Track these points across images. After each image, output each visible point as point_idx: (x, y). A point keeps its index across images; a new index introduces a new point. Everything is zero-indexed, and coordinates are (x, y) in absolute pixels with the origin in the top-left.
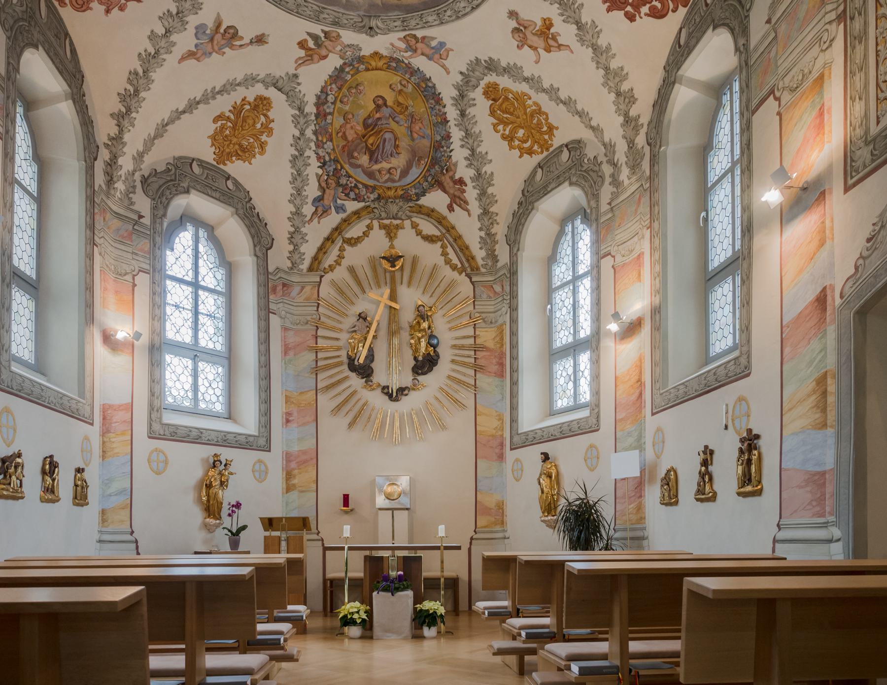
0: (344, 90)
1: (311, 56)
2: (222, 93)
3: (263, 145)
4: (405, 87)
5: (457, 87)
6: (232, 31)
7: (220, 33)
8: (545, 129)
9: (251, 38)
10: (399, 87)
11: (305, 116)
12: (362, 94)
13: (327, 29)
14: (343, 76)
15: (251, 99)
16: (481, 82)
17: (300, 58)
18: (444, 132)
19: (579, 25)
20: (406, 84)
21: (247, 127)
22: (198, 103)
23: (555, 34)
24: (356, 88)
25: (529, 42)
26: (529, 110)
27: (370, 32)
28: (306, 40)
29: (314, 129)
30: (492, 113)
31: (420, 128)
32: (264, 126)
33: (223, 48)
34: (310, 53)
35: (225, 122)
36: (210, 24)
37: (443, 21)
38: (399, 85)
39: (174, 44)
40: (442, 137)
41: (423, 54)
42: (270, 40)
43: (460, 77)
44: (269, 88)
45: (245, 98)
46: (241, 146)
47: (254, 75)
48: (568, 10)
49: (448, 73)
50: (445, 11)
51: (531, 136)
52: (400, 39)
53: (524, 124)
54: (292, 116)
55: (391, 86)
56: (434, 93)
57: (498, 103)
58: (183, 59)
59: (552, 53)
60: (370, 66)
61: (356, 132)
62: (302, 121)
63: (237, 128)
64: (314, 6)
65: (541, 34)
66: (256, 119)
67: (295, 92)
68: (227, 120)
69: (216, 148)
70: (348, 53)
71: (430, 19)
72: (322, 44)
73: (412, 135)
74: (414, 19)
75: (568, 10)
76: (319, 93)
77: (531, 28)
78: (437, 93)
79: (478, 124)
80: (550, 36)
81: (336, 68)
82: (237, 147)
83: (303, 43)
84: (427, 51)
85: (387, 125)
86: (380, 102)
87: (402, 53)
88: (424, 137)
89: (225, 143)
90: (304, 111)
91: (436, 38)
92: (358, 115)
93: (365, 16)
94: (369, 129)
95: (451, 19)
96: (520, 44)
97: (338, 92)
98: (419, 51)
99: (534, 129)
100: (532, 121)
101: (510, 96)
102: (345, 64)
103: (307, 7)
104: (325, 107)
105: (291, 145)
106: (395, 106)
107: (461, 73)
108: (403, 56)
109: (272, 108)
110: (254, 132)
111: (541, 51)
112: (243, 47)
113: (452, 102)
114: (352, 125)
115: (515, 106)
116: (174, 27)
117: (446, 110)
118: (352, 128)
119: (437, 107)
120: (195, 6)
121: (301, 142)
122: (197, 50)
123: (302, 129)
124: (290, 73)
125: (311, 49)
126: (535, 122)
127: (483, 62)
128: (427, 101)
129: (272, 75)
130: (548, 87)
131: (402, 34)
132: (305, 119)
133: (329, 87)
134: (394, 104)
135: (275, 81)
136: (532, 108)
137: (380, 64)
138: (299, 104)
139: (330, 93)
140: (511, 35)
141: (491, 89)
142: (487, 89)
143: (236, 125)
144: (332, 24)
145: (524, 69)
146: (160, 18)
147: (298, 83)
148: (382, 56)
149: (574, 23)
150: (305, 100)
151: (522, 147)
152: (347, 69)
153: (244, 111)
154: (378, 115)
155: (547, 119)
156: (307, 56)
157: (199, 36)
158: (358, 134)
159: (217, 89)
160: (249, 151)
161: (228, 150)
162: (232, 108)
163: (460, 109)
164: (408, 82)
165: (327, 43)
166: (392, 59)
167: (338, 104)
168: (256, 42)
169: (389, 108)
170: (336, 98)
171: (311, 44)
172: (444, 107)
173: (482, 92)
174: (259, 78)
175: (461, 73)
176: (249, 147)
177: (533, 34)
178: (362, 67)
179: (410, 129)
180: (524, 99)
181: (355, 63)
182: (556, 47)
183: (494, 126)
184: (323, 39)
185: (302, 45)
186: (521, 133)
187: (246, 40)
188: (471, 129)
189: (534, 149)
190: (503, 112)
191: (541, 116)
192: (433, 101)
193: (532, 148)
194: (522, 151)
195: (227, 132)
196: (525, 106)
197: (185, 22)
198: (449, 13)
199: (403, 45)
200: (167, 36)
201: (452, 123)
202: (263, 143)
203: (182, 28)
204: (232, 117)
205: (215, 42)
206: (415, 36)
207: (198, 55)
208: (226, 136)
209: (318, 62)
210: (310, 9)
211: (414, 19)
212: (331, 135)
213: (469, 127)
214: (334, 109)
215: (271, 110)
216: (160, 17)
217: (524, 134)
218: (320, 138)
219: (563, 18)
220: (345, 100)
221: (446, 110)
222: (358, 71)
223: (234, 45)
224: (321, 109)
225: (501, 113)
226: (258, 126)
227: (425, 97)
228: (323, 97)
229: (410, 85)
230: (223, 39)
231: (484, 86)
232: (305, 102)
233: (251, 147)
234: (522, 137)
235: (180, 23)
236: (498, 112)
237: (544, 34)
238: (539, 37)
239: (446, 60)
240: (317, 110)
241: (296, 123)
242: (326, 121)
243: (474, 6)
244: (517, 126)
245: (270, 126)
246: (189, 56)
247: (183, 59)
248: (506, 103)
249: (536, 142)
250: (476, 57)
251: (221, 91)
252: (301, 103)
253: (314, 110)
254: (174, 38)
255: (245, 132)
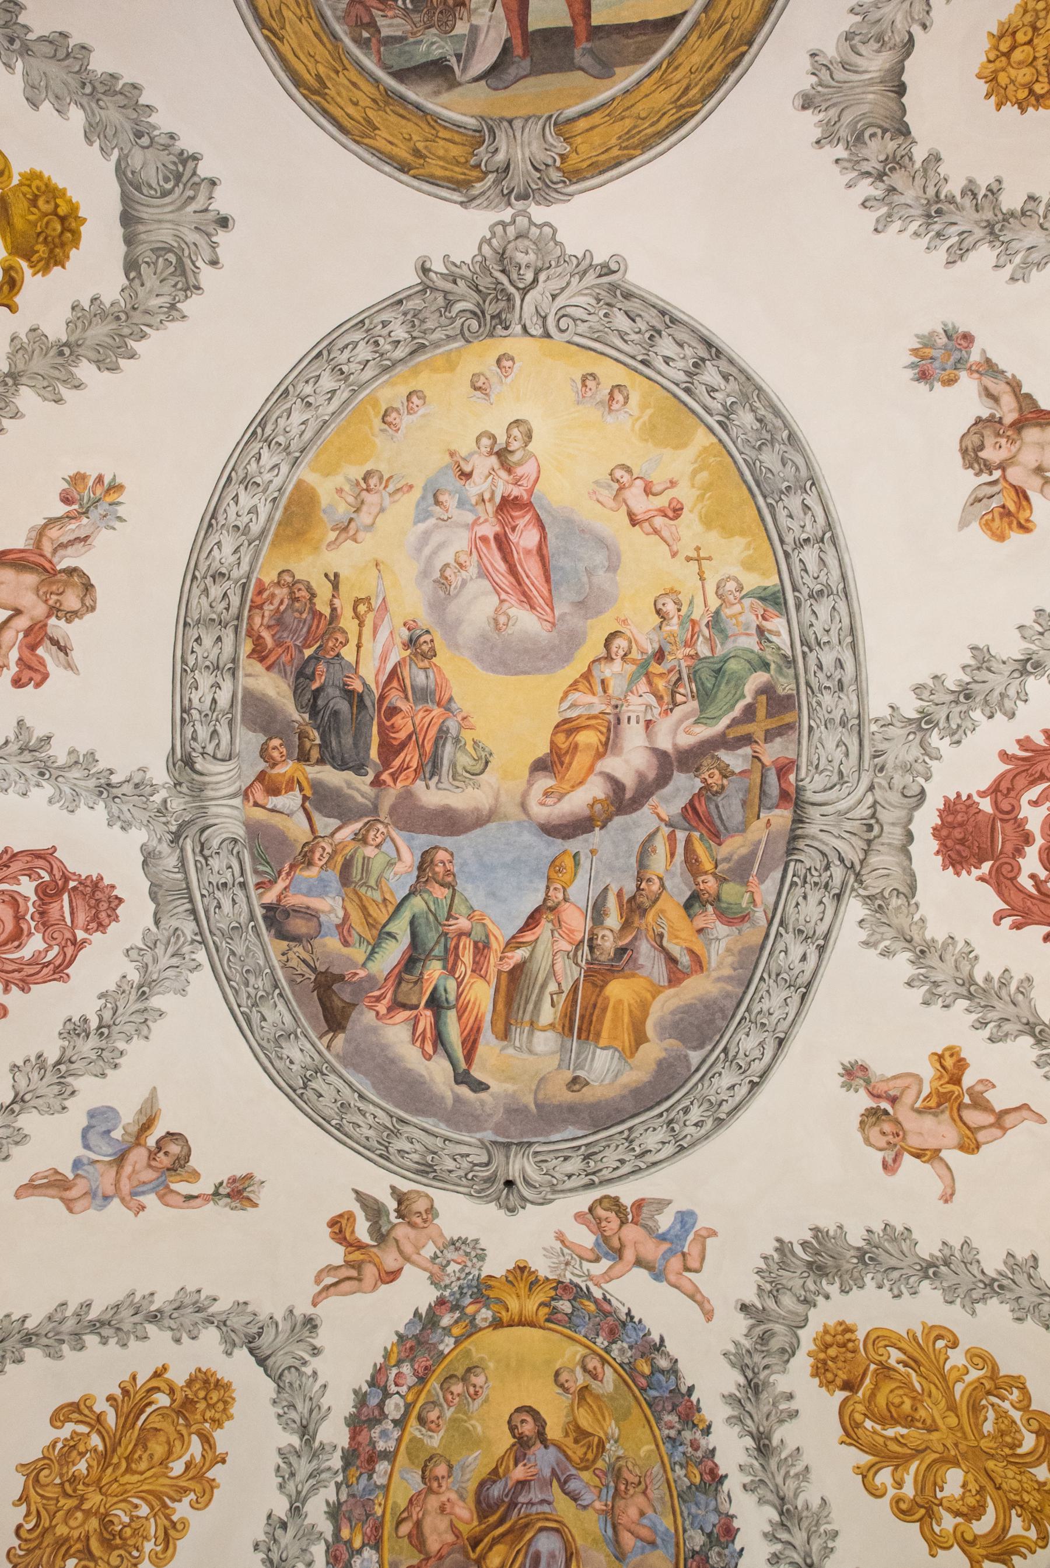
0: (433, 1384)
1: (358, 1266)
2: (106, 1331)
3: (172, 1532)
4: (595, 1377)
5: (739, 1360)
6: (174, 1149)
7: (145, 1146)
8: (1029, 1442)
9: (217, 1182)
10: (581, 1379)
11: (315, 1455)
12: (479, 1401)
13: (405, 1186)
14: (434, 1338)
15: (179, 1376)
16: (800, 1332)
17: (331, 1269)
18: (713, 1518)
19: (1038, 1029)
20: (599, 1370)
21: (143, 1466)
22: (28, 1339)
23: (980, 1088)
24: (464, 1379)
25: (914, 1141)
26: (959, 1388)
27: (507, 1197)
28: (350, 1216)
29: (332, 1498)
30: (851, 1434)
31: (642, 1514)
32: (192, 1473)
33: (143, 1193)
34: (357, 1256)
35: (84, 1429)
36: (128, 1115)
37: (684, 1144)
38: (579, 1371)
39: (21, 1138)
40: (709, 1535)
41: (639, 1263)
42: (264, 1196)
43: (742, 1323)
44: (236, 1351)
45: (165, 1368)
46: (106, 1522)
47: (203, 1295)
48: (995, 1002)
49: (709, 1315)
50: (686, 1111)
51: (990, 1487)
52: (578, 1216)
53: (956, 1445)
54: (280, 1451)
55: (557, 1374)
56: (676, 1391)
57: (860, 1394)
58: (30, 1188)
59: (983, 1148)
60: (504, 1313)
61: (452, 1525)
62: (303, 1468)
63: (115, 1460)
64: (380, 1113)
65: (939, 1105)
66: (178, 1444)
67: (301, 1374)
68: (92, 1427)
69: (28, 1514)
70: (449, 1269)
71: (651, 1140)
72: (389, 1232)
73: (617, 1542)
74: (613, 1146)
75: (995, 1002)
76: (365, 1388)
77: (908, 1099)
78: (684, 1390)
79: (813, 1476)
80: (967, 1100)
81: (416, 1313)
82: (94, 1523)
83: (344, 1222)
84: (652, 1251)
85: (546, 1508)
86: (528, 1428)
87: (586, 1265)
88: (653, 1544)
89: (62, 1501)
90: (314, 1438)
91: (669, 1202)
92: (463, 1468)
93: (494, 1143)
94: (493, 1519)
95: (703, 1131)
96: (890, 1156)
97: (415, 1390)
98: (629, 1255)
99: (992, 1457)
100: (977, 1427)
101: (895, 1356)
102: (441, 1302)
103: (363, 1113)
104: (375, 1433)
105: (256, 1547)
106: (569, 1442)
107: (744, 1308)
108: (590, 1277)
109: (230, 1417)
110: (160, 1485)
111: (952, 1156)
112: (193, 1203)
113: (728, 1411)
114: (444, 1499)
115: (914, 1390)
116: (39, 1092)
117: (712, 1441)
118: (442, 1509)
119: (687, 1435)
120: (105, 1054)
121: (286, 1538)
122: (77, 1176)
123: (299, 1493)
124: (296, 1312)
125: (360, 1246)
126: (988, 1427)
127: (798, 1250)
128: (658, 1420)
129: (250, 1309)
130: (1002, 1268)
131: (584, 1200)
132: (315, 1462)
133: (394, 1371)
134: (567, 1435)
135: (253, 1330)
136: (968, 1379)
137: (531, 1306)
138: (306, 1415)
139: (393, 1389)
140: (859, 1137)
141: (832, 1352)
142: (822, 1356)
143: (114, 1450)
144: (417, 1172)
145: (915, 1236)
146: (15, 1068)
147: (315, 1348)
148: (537, 1280)
149: (1022, 1032)
150: (325, 1402)
151: (969, 1537)
152: (446, 1320)
153: (149, 1410)
154: (519, 1473)
155: (1025, 1404)
156: (348, 1264)
157: (94, 1138)
158: (458, 1535)
159: (93, 1314)
160: (124, 1546)
161: (61, 1530)
162: (118, 1392)
163: (754, 1430)
164: (604, 1361)
165: (402, 1232)
166: (562, 1288)
167: (413, 1427)
168: (228, 1195)
169: (552, 1449)
170: (409, 1407)
171: (362, 1230)
172: (707, 1431)
173: (809, 1370)
174: (215, 1308)
175: (744, 1308)
176: (128, 1531)
177: (919, 1111)
178: (485, 1315)
179: (611, 1516)
180: (937, 1353)
181: (468, 1300)
182: (991, 1125)
183: (864, 1477)
184: (393, 1216)
185: (340, 1228)
186: (954, 1481)
187: (204, 1188)
188: (796, 1496)
189: (1011, 1533)
190: (883, 1421)
191: (1003, 1399)
192: (673, 1418)
193: (1005, 1530)
194: (973, 1550)
195: (82, 1466)
196: (944, 1378)
197: (69, 1090)
198: (695, 1114)
199: (585, 1238)
200: (13, 1111)
201: (733, 1484)
202: (174, 1524)
203: (56, 1103)
204: (111, 1419)
205: (128, 1169)
206: (615, 1204)
207: (73, 1193)
208: (74, 1479)
209: (375, 1288)
210: (370, 1119)
211: (613, 1146)
212: (378, 1527)
213: (789, 1488)
214: (399, 1440)
215: (227, 1424)
216: (15, 1066)
217: (964, 1486)
218: (345, 1533)
219: (986, 1032)
220: (433, 1415)
221: (712, 1441)
222: (473, 1329)
223: (172, 1191)
224: (363, 1438)
225: (878, 1427)
226: (177, 1467)
227: (650, 1406)
228: (374, 1401)
229: (609, 1371)
230: (150, 1166)
231: (813, 1347)
232: (325, 1408)
233: (135, 1532)
234: (962, 1498)
235: (56, 1089)
236: (868, 1424)
237: (948, 1100)
238: (935, 1115)
239: (697, 1271)
240: (353, 1438)
241: (285, 1474)
242: (370, 1477)
243: (756, 1080)
244: (935, 1461)
245: (210, 1475)
246: (49, 1185)
247: (30, 1188)
248: (887, 1387)
249: (1013, 1505)
250: (779, 1240)
251: (103, 1324)
252: (311, 1411)
253: (343, 1439)
254: (28, 1121)
255: (136, 1478)
